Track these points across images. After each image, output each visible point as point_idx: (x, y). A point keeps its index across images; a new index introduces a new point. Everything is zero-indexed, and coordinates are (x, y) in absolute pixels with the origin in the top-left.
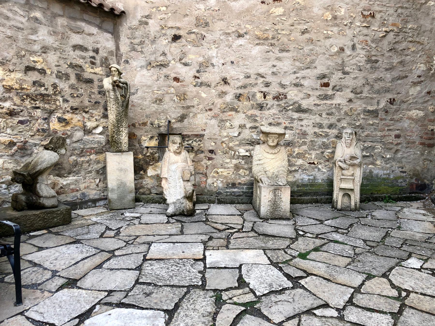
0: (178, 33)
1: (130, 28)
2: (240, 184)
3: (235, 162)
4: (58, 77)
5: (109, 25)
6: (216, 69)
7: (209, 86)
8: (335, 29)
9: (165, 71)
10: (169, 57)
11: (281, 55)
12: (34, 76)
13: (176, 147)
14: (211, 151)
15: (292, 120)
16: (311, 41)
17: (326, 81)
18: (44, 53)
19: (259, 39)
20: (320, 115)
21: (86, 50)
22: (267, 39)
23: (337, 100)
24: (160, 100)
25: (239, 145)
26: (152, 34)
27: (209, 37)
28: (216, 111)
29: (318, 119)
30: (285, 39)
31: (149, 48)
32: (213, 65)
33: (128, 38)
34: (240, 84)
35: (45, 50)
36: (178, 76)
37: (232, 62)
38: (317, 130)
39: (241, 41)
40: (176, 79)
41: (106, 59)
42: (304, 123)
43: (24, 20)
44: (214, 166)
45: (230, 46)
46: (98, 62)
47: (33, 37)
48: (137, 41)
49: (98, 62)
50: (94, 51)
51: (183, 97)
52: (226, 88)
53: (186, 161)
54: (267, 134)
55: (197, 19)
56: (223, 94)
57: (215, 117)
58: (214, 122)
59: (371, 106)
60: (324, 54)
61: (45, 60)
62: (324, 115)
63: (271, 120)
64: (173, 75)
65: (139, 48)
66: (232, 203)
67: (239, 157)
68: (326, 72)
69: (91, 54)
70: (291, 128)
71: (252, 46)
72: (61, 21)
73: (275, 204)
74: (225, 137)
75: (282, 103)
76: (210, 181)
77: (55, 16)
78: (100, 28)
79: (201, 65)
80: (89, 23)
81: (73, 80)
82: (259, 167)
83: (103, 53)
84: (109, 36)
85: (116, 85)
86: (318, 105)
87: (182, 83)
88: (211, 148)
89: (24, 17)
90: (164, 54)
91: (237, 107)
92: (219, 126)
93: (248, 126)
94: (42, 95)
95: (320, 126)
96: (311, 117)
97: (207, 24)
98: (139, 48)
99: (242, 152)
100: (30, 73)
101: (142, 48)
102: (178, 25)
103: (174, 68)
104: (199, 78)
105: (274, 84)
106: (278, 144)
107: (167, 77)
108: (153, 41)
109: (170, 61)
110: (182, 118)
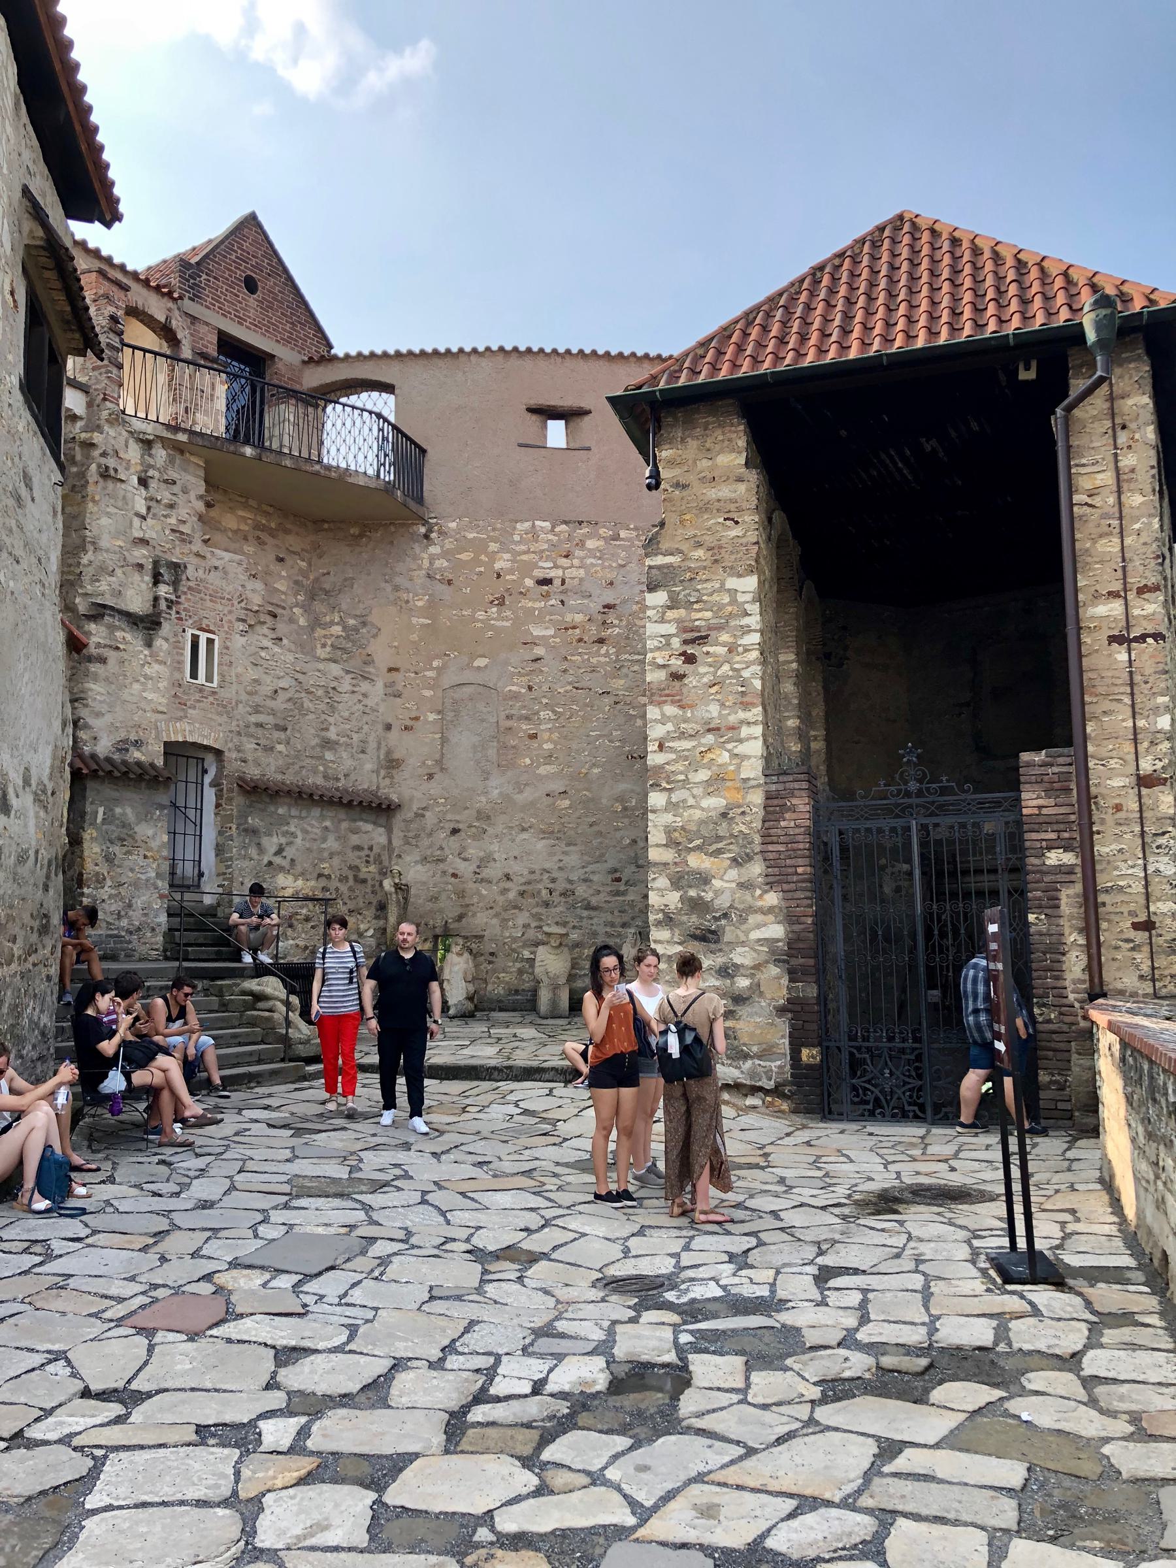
1: (404, 821)
2: (523, 990)
3: (518, 965)
4: (340, 880)
5: (382, 821)
6: (498, 865)
7: (490, 882)
8: (626, 821)
9: (441, 866)
10: (447, 851)
11: (567, 849)
13: (459, 948)
14: (492, 954)
15: (581, 918)
16: (600, 833)
17: (617, 875)
19: (544, 832)
20: (612, 913)
22: (552, 832)
23: (630, 897)
24: (437, 898)
26: (429, 827)
27: (490, 830)
28: (498, 909)
29: (610, 918)
30: (572, 833)
31: (426, 842)
32: (494, 860)
34: (523, 880)
35: (331, 856)
38: (608, 929)
39: (525, 835)
40: (454, 875)
41: (379, 855)
42: (595, 921)
44: (495, 971)
45: (513, 841)
46: (371, 859)
47: (324, 846)
48: (411, 834)
49: (371, 859)
51: (461, 894)
52: (508, 885)
53: (467, 962)
54: (549, 934)
55: (479, 812)
56: (505, 891)
57: (497, 915)
58: (495, 921)
60: (615, 846)
61: (331, 866)
62: (616, 913)
63: (558, 919)
64: (451, 871)
65: (414, 842)
66: (514, 1010)
67: (523, 960)
68: (618, 866)
69: (367, 852)
70: (580, 928)
73: (554, 1003)
75: (570, 900)
76: (490, 987)
77: (340, 821)
78: (375, 823)
79: (482, 860)
80: (366, 821)
81: (351, 882)
82: (542, 969)
83: (376, 850)
84: (382, 830)
85: (397, 887)
86: (609, 902)
90: (441, 848)
93: (533, 925)
95: (612, 925)
96: (602, 915)
97: (488, 817)
98: (414, 842)
99: (526, 954)
102: (458, 818)
103: (451, 863)
105: (560, 880)
106: (561, 944)
107: (444, 872)
108: (430, 835)
110: (460, 917)
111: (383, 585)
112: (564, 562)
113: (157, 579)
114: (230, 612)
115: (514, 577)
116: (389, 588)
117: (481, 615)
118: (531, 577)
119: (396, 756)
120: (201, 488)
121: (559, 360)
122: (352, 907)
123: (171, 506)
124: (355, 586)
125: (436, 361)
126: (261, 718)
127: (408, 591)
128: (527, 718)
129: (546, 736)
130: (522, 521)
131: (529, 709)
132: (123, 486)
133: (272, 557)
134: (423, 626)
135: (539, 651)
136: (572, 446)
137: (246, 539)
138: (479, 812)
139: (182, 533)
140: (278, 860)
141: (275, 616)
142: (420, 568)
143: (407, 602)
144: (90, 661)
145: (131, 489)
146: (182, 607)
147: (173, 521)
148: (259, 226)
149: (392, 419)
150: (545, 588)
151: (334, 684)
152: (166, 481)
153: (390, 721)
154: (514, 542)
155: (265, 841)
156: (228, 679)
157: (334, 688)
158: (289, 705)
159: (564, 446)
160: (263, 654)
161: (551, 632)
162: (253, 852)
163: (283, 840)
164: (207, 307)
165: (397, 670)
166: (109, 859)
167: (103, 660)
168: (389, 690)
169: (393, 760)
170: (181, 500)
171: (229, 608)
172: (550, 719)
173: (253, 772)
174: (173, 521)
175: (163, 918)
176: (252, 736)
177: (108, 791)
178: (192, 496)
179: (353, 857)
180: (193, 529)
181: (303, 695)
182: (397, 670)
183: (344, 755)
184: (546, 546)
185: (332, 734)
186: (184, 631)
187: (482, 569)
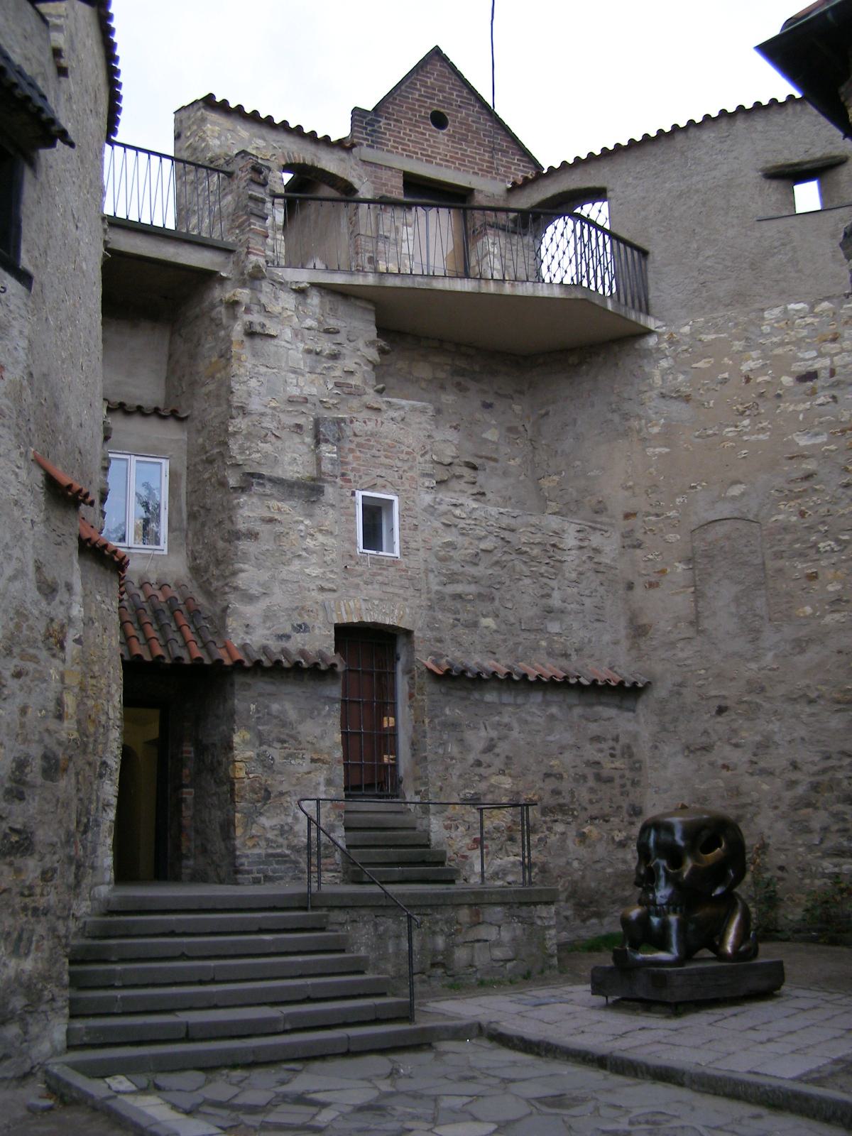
0: (724, 703)
6: (781, 751)
7: (772, 773)
10: (715, 737)
12: (551, 784)
18: (561, 753)
19: (839, 702)
21: (605, 740)
25: (822, 858)
33: (656, 715)
34: (816, 768)
35: (562, 749)
36: (726, 762)
37: (803, 739)
40: (725, 767)
41: (629, 747)
43: (541, 720)
46: (618, 752)
47: (551, 738)
49: (618, 752)
50: (613, 740)
59: (846, 234)
64: (720, 762)
69: (611, 743)
71: (829, 713)
72: (578, 711)
74: (801, 846)
77: (570, 707)
78: (620, 707)
80: (607, 705)
81: (591, 782)
87: (733, 772)
88: (780, 863)
89: (541, 717)
91: (814, 802)
92: (790, 830)
93: (835, 828)
94: (561, 806)
100: (547, 780)
101: (675, 727)
102: (724, 693)
104: (756, 763)
109: (714, 742)
111: (609, 416)
112: (831, 348)
113: (318, 440)
114: (411, 468)
115: (766, 378)
116: (616, 418)
117: (729, 432)
118: (789, 374)
119: (643, 620)
120: (372, 332)
121: (798, 107)
122: (595, 813)
123: (334, 357)
124: (579, 422)
125: (651, 149)
126: (459, 588)
127: (639, 417)
128: (802, 555)
129: (830, 573)
130: (771, 308)
131: (804, 542)
132: (275, 342)
133: (477, 404)
134: (660, 455)
135: (810, 466)
136: (829, 206)
137: (443, 387)
138: (749, 682)
139: (349, 386)
140: (486, 758)
141: (474, 468)
142: (652, 388)
143: (639, 431)
144: (238, 539)
145: (283, 343)
146: (350, 467)
147: (338, 373)
148: (445, 59)
149: (607, 226)
150: (810, 384)
151: (555, 540)
152: (327, 331)
153: (631, 578)
154: (762, 335)
155: (470, 736)
156: (413, 545)
157: (554, 545)
158: (495, 570)
159: (819, 208)
160: (458, 512)
161: (822, 439)
162: (453, 749)
163: (494, 734)
164: (388, 151)
165: (634, 514)
166: (265, 762)
167: (253, 535)
168: (628, 542)
169: (640, 627)
170: (347, 349)
171: (409, 464)
172: (833, 551)
173: (454, 656)
174: (338, 373)
175: (340, 835)
176: (449, 610)
177: (261, 685)
178: (361, 344)
179: (591, 752)
180: (365, 382)
181: (514, 556)
182: (634, 514)
183: (575, 625)
184: (804, 333)
185: (556, 601)
186: (353, 494)
187: (726, 375)
